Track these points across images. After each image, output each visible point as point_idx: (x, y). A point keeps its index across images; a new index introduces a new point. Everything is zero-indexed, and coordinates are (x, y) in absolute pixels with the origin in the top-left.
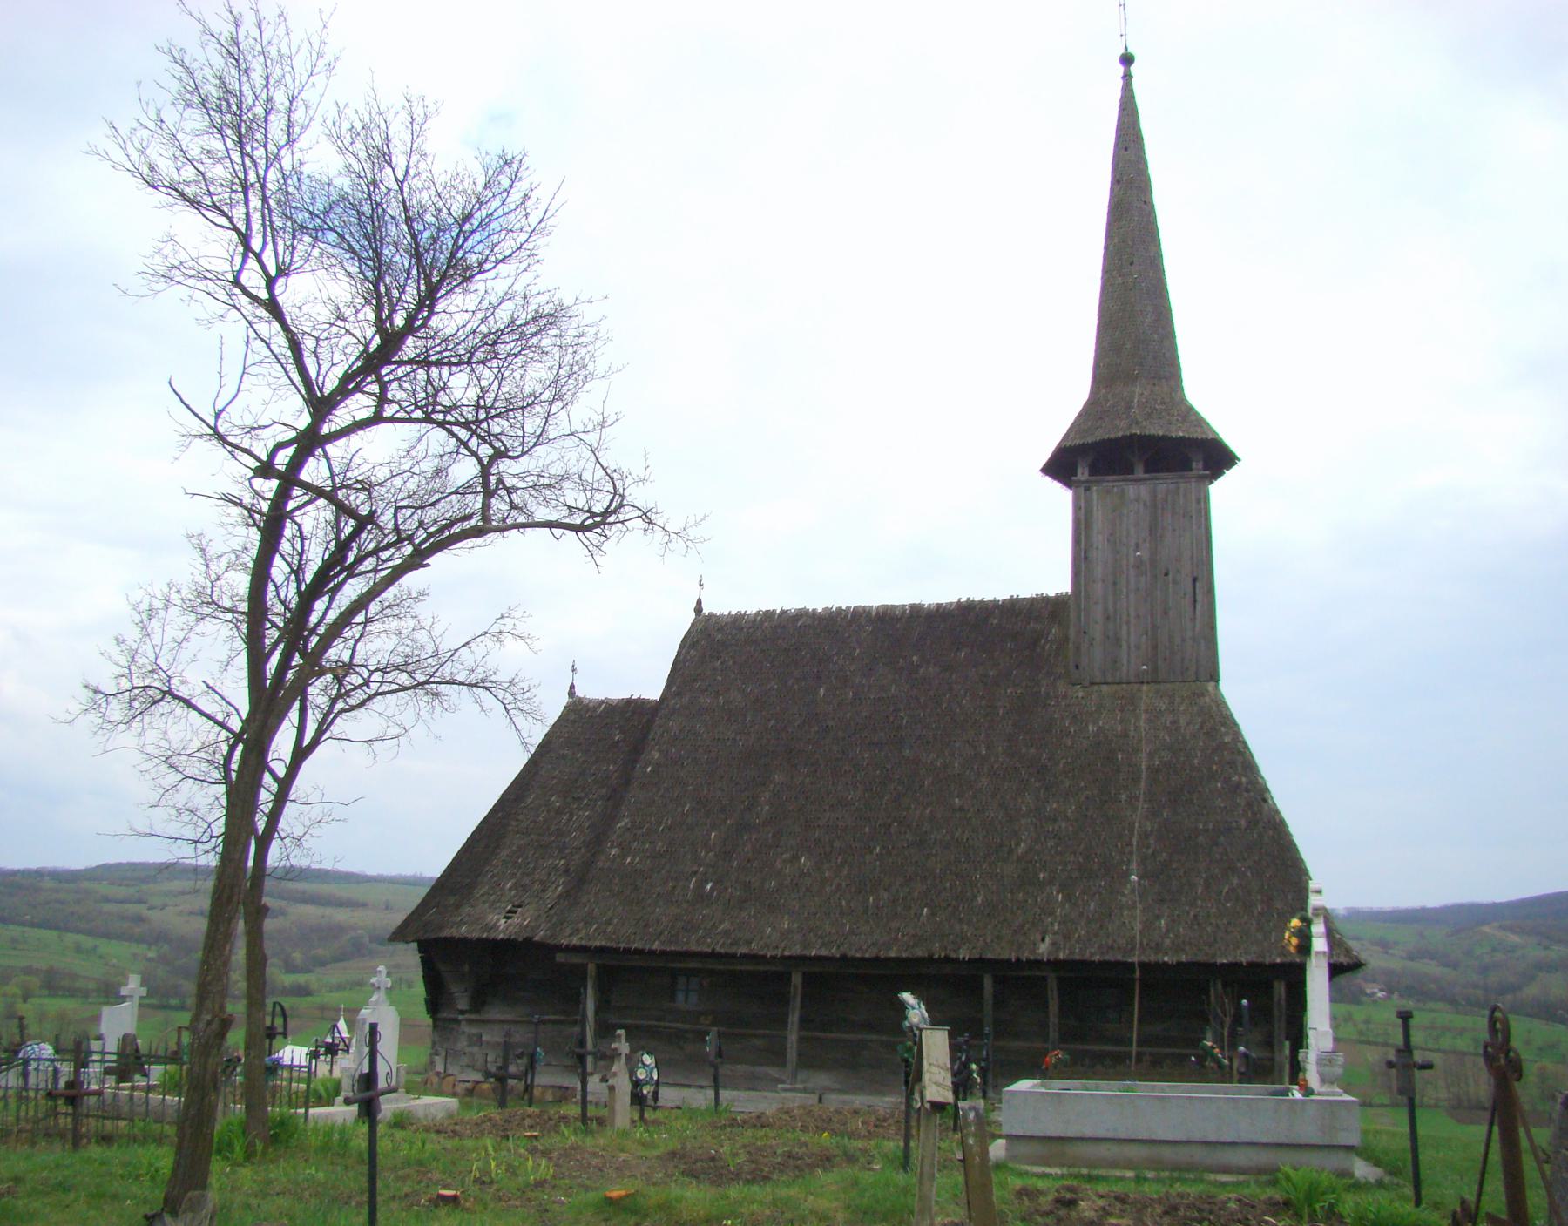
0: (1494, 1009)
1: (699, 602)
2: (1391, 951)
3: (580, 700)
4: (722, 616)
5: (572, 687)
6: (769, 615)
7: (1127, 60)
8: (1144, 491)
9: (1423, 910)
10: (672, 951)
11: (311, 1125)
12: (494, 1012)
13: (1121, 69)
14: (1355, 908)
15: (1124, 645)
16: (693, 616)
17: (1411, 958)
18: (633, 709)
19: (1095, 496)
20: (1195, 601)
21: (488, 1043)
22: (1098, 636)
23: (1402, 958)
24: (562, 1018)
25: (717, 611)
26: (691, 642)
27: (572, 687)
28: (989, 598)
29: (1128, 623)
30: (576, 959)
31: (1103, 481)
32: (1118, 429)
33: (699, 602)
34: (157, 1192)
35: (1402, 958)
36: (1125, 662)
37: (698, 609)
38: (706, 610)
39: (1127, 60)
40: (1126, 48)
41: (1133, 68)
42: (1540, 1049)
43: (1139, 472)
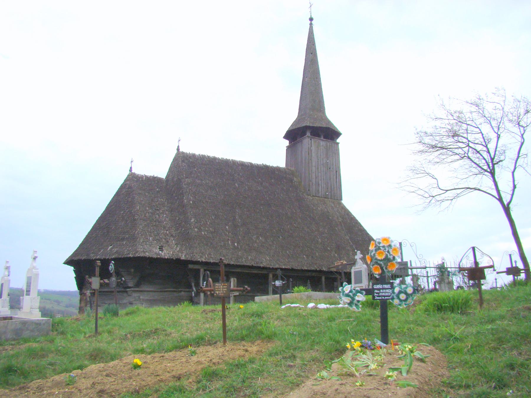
0: (215, 311)
1: (178, 147)
2: (60, 304)
3: (134, 174)
4: (186, 153)
5: (131, 168)
6: (204, 157)
7: (311, 19)
8: (322, 143)
9: (69, 291)
10: (239, 265)
11: (507, 285)
12: (145, 288)
13: (309, 22)
14: (46, 290)
15: (320, 187)
16: (176, 152)
17: (67, 307)
18: (153, 181)
19: (313, 142)
20: (336, 177)
21: (143, 300)
22: (314, 182)
23: (64, 306)
24: (175, 290)
25: (185, 151)
26: (175, 160)
27: (131, 168)
28: (271, 165)
29: (321, 180)
30: (196, 267)
31: (315, 138)
32: (307, 123)
33: (178, 147)
34: (27, 366)
35: (64, 306)
36: (321, 191)
37: (178, 149)
38: (181, 150)
39: (311, 19)
40: (311, 16)
41: (313, 22)
42: (425, 300)
43: (322, 138)
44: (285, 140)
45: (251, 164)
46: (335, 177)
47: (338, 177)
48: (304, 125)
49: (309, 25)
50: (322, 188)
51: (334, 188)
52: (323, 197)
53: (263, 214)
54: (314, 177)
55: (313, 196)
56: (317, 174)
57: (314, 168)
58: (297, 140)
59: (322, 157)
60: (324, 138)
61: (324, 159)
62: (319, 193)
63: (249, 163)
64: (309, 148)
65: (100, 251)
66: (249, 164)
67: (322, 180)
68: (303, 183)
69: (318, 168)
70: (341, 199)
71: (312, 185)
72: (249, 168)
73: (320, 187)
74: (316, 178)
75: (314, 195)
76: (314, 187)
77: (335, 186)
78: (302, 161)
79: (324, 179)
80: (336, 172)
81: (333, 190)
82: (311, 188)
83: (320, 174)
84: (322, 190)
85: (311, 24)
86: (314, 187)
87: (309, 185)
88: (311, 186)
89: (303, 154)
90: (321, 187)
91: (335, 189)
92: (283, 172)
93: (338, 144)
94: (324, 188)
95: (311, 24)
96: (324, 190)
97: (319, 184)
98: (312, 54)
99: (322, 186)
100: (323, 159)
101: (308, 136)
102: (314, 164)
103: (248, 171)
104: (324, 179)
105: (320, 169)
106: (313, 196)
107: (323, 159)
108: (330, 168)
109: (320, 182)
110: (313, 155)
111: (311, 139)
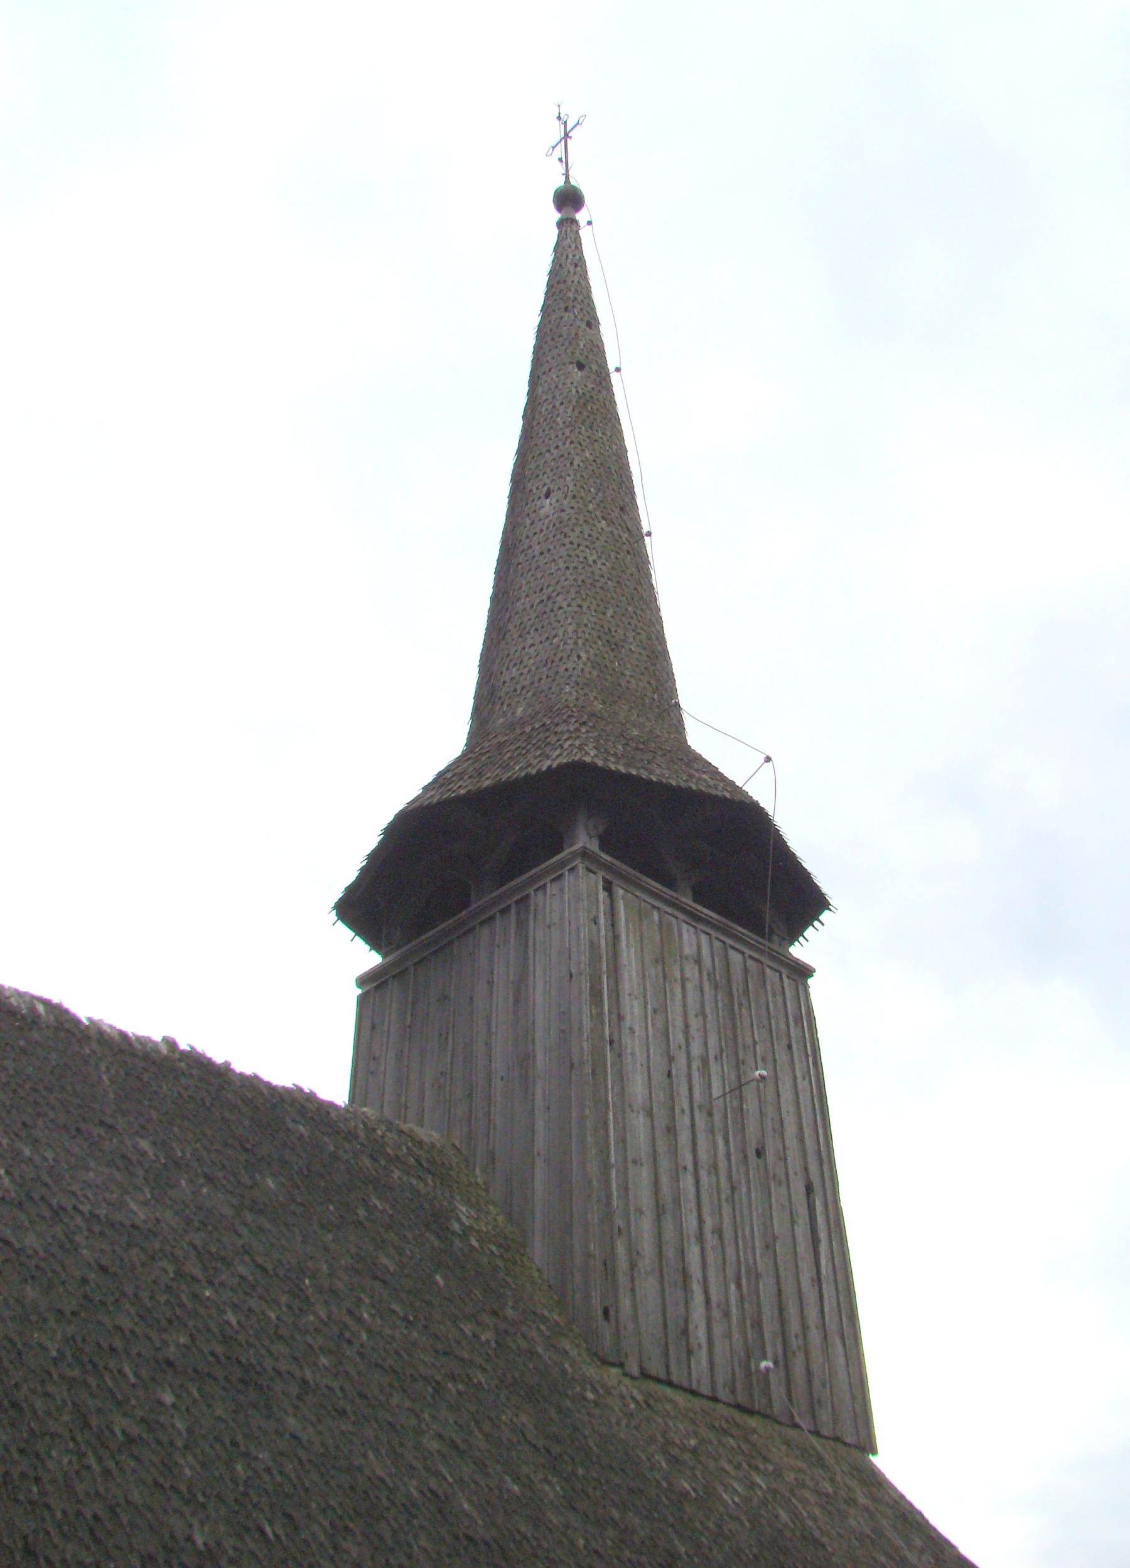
8: (689, 938)
29: (701, 1238)
41: (581, 217)
44: (344, 932)
45: (58, 1011)
46: (802, 1229)
47: (823, 1235)
48: (556, 759)
49: (555, 232)
50: (716, 1313)
51: (805, 1327)
52: (723, 1394)
53: (188, 1468)
54: (643, 1196)
55: (645, 1375)
56: (664, 1179)
57: (639, 1123)
58: (466, 905)
59: (696, 1049)
60: (698, 898)
61: (714, 1067)
62: (690, 1352)
63: (46, 1003)
64: (593, 946)
65: (749, 1520)
66: (41, 1008)
67: (711, 1240)
68: (539, 1252)
69: (671, 1130)
70: (869, 1446)
71: (633, 1266)
72: (36, 1035)
73: (698, 1298)
74: (659, 1211)
75: (655, 1367)
76: (649, 1287)
77: (812, 1314)
78: (525, 1060)
79: (719, 1232)
80: (809, 1189)
81: (794, 1343)
82: (626, 1303)
83: (688, 1181)
84: (718, 1329)
85: (568, 229)
86: (649, 1287)
87: (608, 1268)
88: (623, 1280)
89: (539, 998)
90: (708, 1301)
91: (815, 1337)
92: (351, 1136)
93: (803, 972)
94: (727, 1314)
95: (568, 229)
96: (728, 1335)
97: (686, 1276)
98: (581, 366)
99: (714, 1300)
100: (705, 1061)
101: (585, 854)
102: (637, 1087)
103: (24, 1051)
104: (719, 1232)
105: (684, 1137)
106: (645, 1375)
107: (705, 1061)
108: (759, 1153)
109: (693, 1254)
110: (633, 1009)
111: (608, 887)
